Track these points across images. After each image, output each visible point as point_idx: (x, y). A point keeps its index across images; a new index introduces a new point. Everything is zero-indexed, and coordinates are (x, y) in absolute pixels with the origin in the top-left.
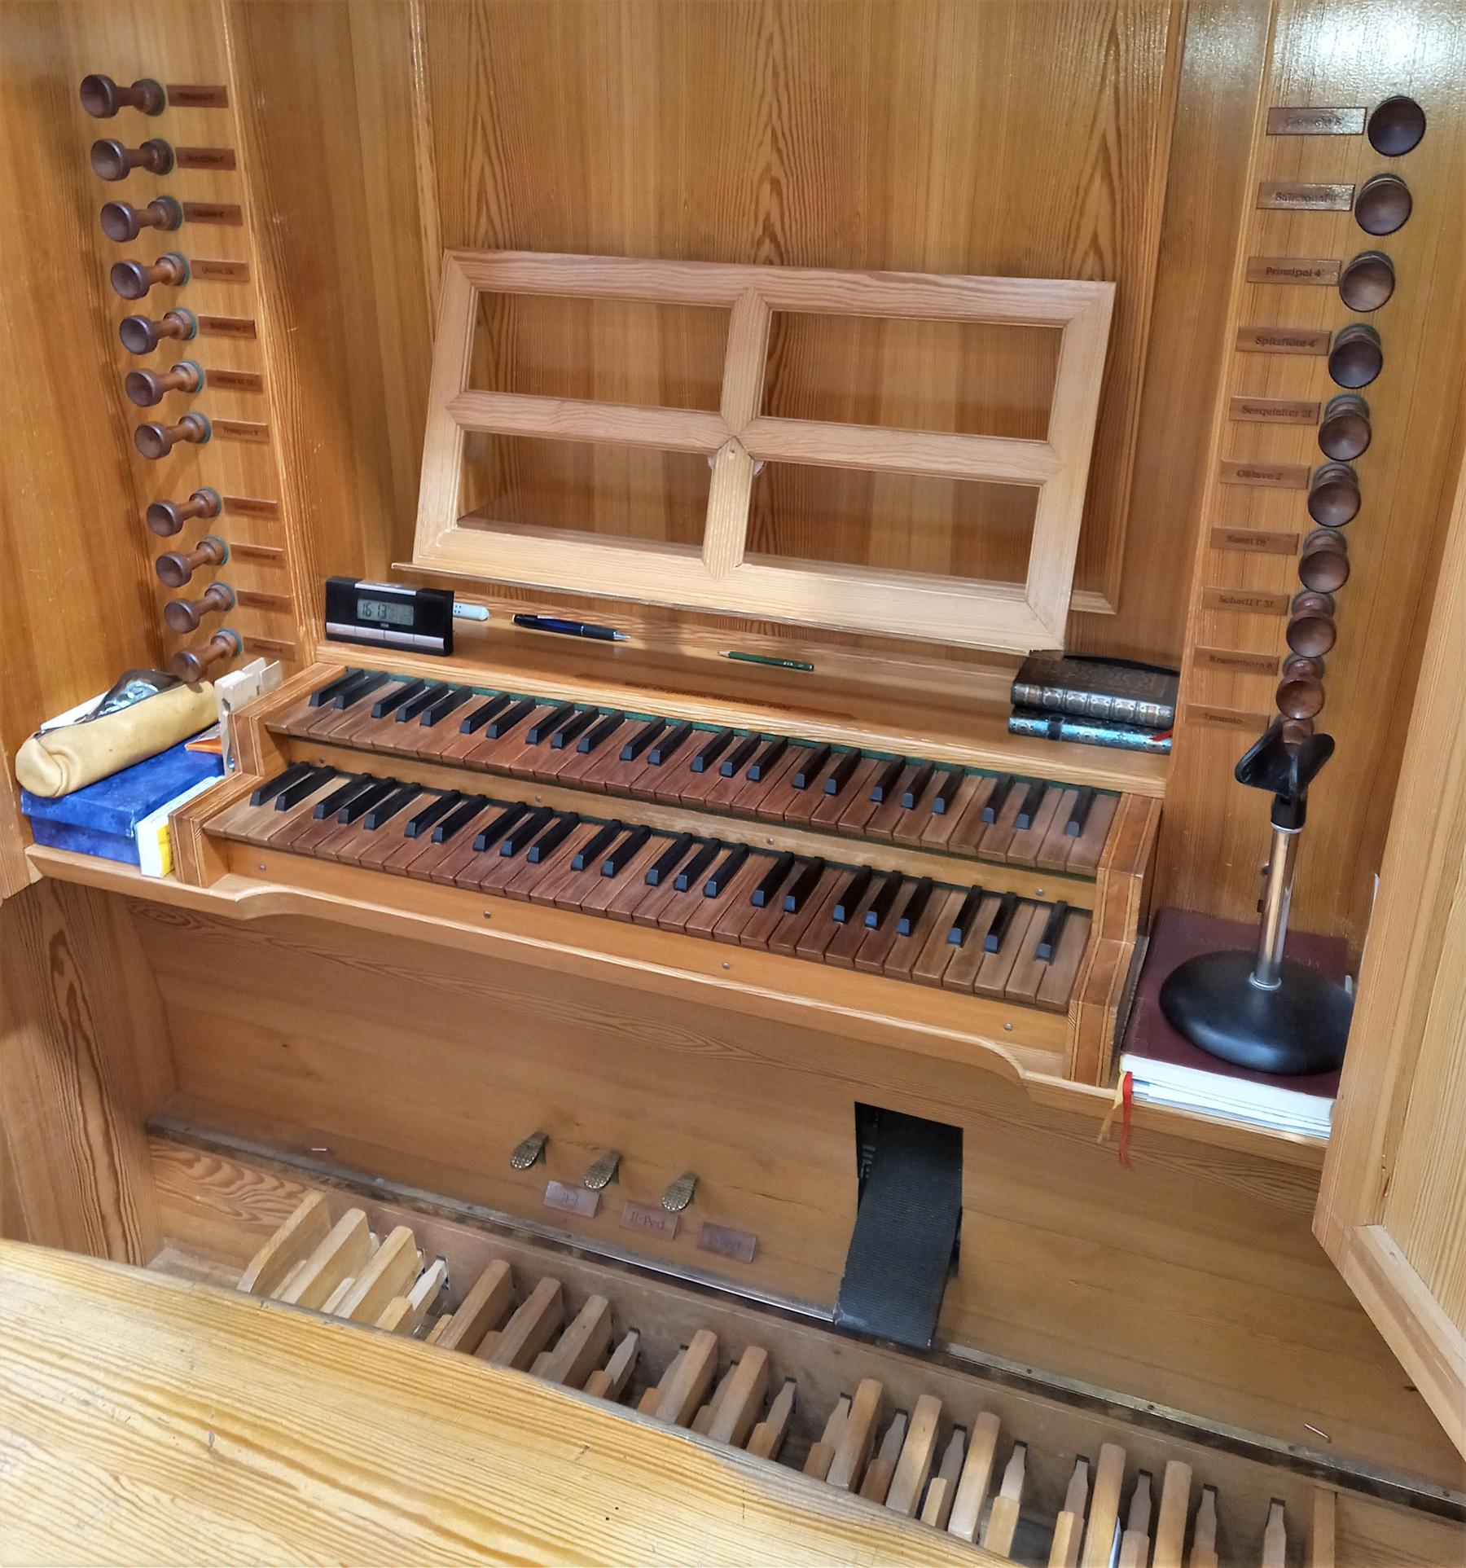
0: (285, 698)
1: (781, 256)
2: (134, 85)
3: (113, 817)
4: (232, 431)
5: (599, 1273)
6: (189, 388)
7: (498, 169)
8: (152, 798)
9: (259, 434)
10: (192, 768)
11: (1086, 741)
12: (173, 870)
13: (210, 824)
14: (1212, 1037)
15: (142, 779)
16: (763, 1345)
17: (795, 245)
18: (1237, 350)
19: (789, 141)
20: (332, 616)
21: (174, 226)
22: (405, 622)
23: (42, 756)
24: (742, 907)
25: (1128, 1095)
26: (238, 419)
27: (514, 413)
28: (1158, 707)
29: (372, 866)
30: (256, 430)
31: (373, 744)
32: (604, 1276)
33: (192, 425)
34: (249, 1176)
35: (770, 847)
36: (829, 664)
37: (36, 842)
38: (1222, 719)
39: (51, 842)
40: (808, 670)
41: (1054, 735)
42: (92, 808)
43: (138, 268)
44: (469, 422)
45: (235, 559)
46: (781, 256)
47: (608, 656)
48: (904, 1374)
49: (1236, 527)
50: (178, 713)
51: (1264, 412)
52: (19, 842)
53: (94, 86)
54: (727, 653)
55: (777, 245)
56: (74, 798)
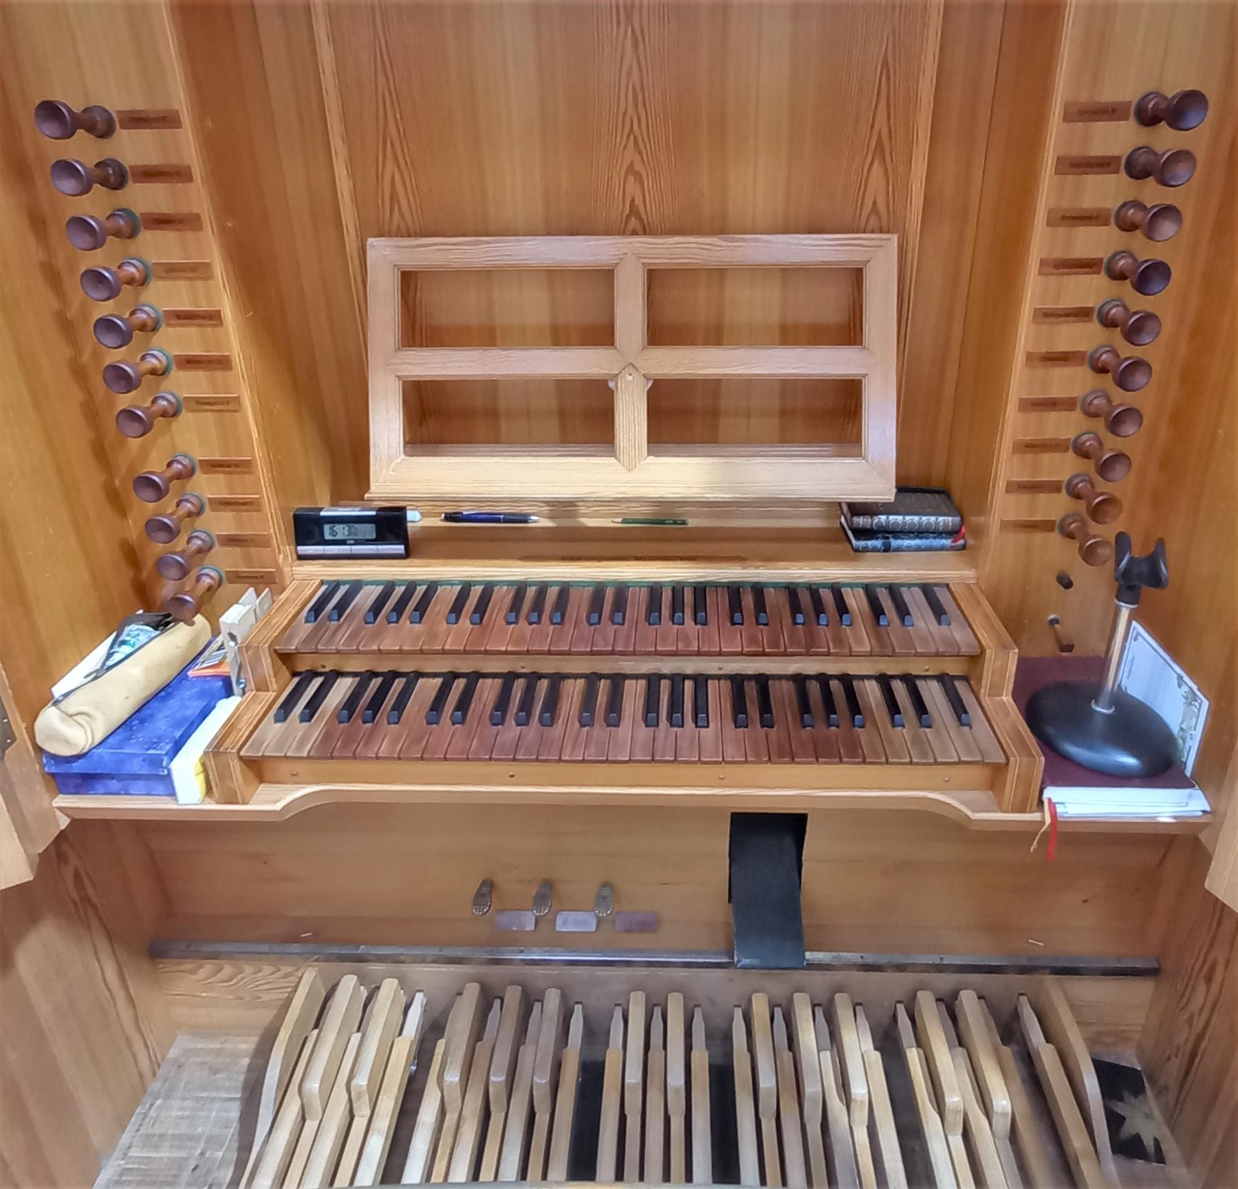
0: (281, 620)
1: (645, 229)
2: (84, 111)
5: (550, 972)
6: (160, 373)
7: (406, 177)
8: (178, 734)
9: (229, 405)
11: (909, 549)
12: (209, 790)
13: (247, 751)
15: (159, 716)
20: (299, 542)
21: (133, 234)
23: (63, 721)
30: (227, 401)
33: (165, 403)
34: (248, 969)
37: (61, 792)
41: (887, 549)
42: (121, 756)
43: (110, 274)
46: (645, 229)
48: (778, 985)
50: (178, 648)
52: (46, 797)
53: (50, 110)
54: (620, 520)
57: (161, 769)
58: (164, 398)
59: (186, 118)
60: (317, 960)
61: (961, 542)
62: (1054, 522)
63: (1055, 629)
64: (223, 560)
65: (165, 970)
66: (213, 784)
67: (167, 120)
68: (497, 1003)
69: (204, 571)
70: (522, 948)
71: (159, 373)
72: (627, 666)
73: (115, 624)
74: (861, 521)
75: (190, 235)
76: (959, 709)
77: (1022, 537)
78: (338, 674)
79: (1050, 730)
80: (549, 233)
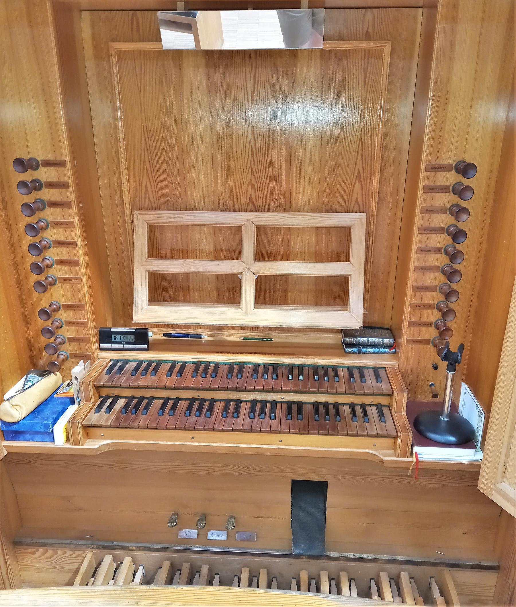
0: (88, 379)
3: (42, 426)
4: (65, 280)
6: (50, 266)
8: (55, 416)
10: (62, 403)
11: (370, 353)
12: (68, 439)
13: (85, 422)
14: (432, 436)
16: (265, 568)
17: (260, 205)
18: (418, 233)
19: (257, 172)
20: (101, 341)
22: (131, 341)
24: (284, 421)
25: (417, 459)
26: (69, 276)
27: (167, 265)
28: (389, 340)
29: (152, 427)
30: (77, 279)
31: (147, 385)
32: (206, 557)
33: (51, 279)
34: (60, 552)
35: (282, 400)
36: (277, 338)
37: (5, 440)
38: (417, 342)
39: (13, 439)
40: (272, 340)
41: (360, 352)
42: (33, 424)
44: (150, 270)
45: (66, 326)
47: (200, 344)
48: (313, 565)
49: (419, 284)
50: (51, 384)
51: (426, 251)
54: (242, 338)
55: (254, 205)
56: (24, 421)
57: (48, 430)
58: (50, 277)
59: (68, 164)
60: (93, 548)
61: (393, 350)
62: (430, 340)
63: (432, 389)
64: (68, 349)
65: (20, 552)
66: (70, 436)
67: (61, 164)
68: (178, 572)
69: (60, 353)
70: (192, 545)
71: (49, 267)
72: (243, 396)
73: (24, 372)
74: (349, 340)
75: (66, 210)
76: (381, 415)
77: (416, 346)
78: (118, 397)
79: (422, 428)
80: (214, 210)
